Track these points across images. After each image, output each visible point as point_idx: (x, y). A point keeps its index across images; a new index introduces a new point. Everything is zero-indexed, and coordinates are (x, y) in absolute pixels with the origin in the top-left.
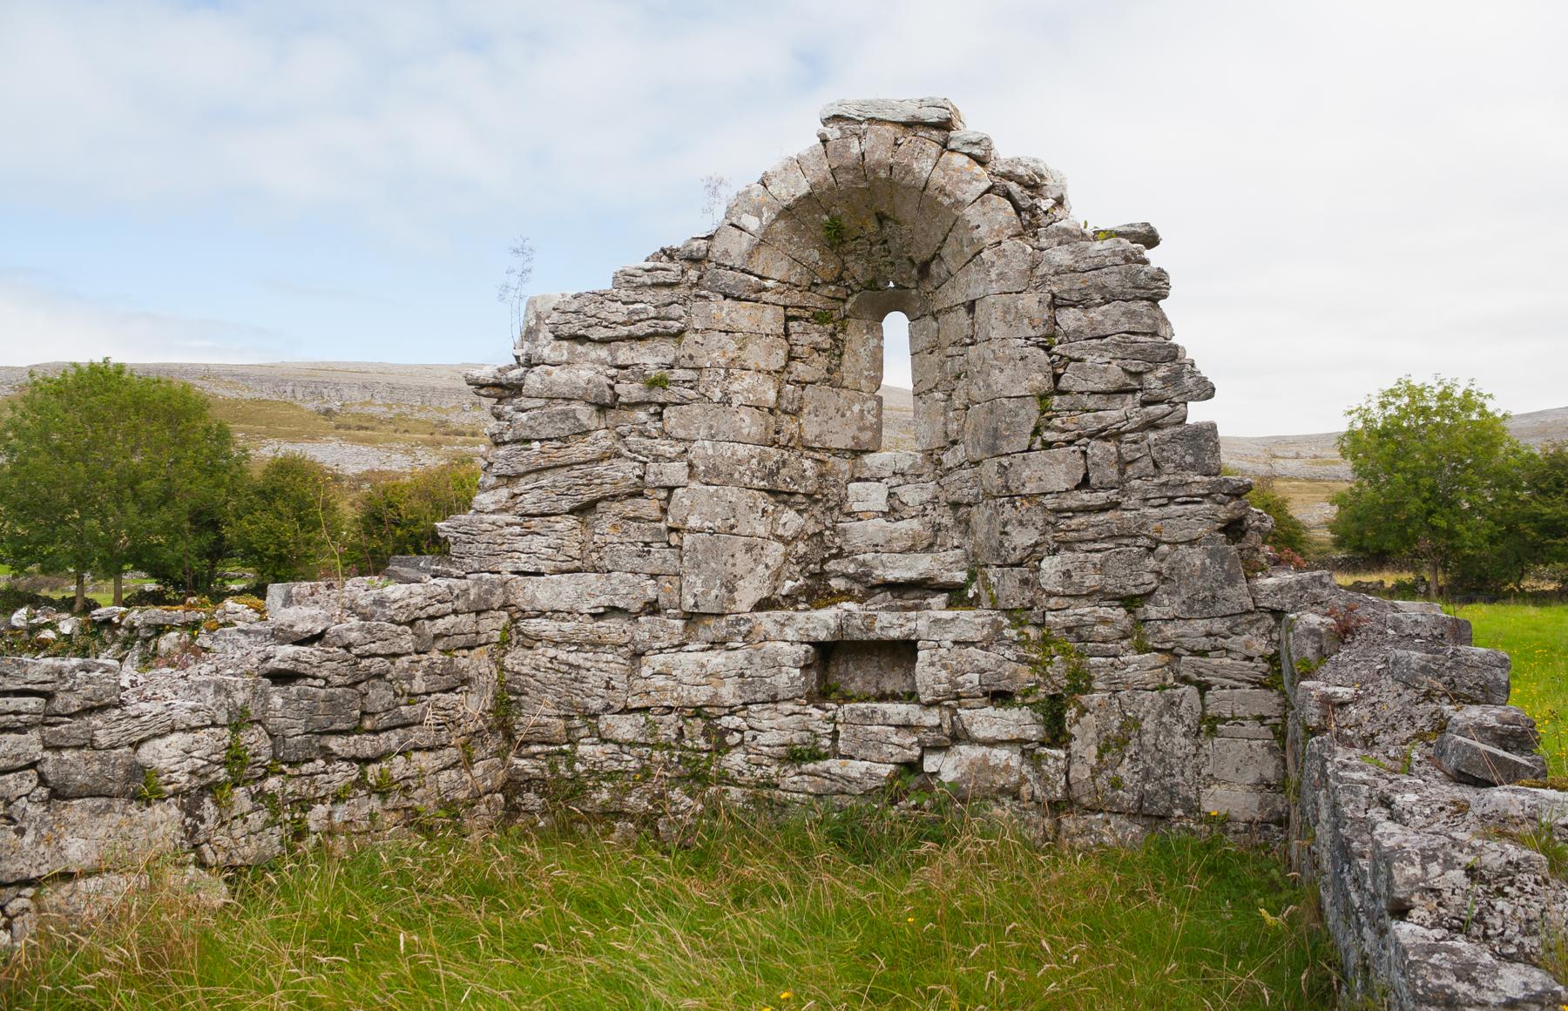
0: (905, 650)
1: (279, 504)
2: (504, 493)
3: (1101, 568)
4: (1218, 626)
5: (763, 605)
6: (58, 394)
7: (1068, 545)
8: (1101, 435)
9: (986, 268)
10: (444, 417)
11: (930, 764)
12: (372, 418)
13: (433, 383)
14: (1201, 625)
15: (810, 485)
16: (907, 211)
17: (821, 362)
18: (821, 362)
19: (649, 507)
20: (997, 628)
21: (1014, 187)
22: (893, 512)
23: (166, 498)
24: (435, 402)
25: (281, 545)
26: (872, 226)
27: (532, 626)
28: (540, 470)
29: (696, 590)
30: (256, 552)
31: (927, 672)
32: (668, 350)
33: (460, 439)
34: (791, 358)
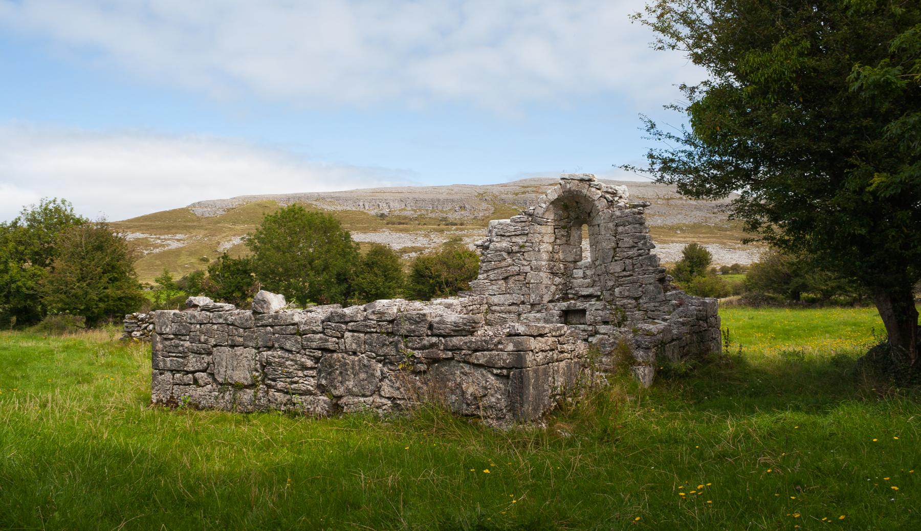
0: (583, 312)
1: (376, 269)
2: (485, 275)
3: (628, 291)
4: (657, 304)
5: (550, 302)
6: (274, 222)
7: (621, 285)
8: (628, 258)
9: (600, 216)
10: (445, 215)
11: (590, 340)
12: (405, 218)
13: (438, 196)
14: (652, 304)
15: (562, 271)
16: (582, 201)
17: (564, 239)
18: (564, 239)
19: (521, 278)
20: (605, 306)
21: (608, 196)
22: (584, 277)
23: (326, 268)
24: (440, 208)
25: (377, 289)
26: (575, 204)
27: (494, 308)
28: (494, 269)
29: (533, 298)
30: (365, 292)
31: (589, 317)
32: (525, 238)
33: (454, 227)
34: (556, 238)
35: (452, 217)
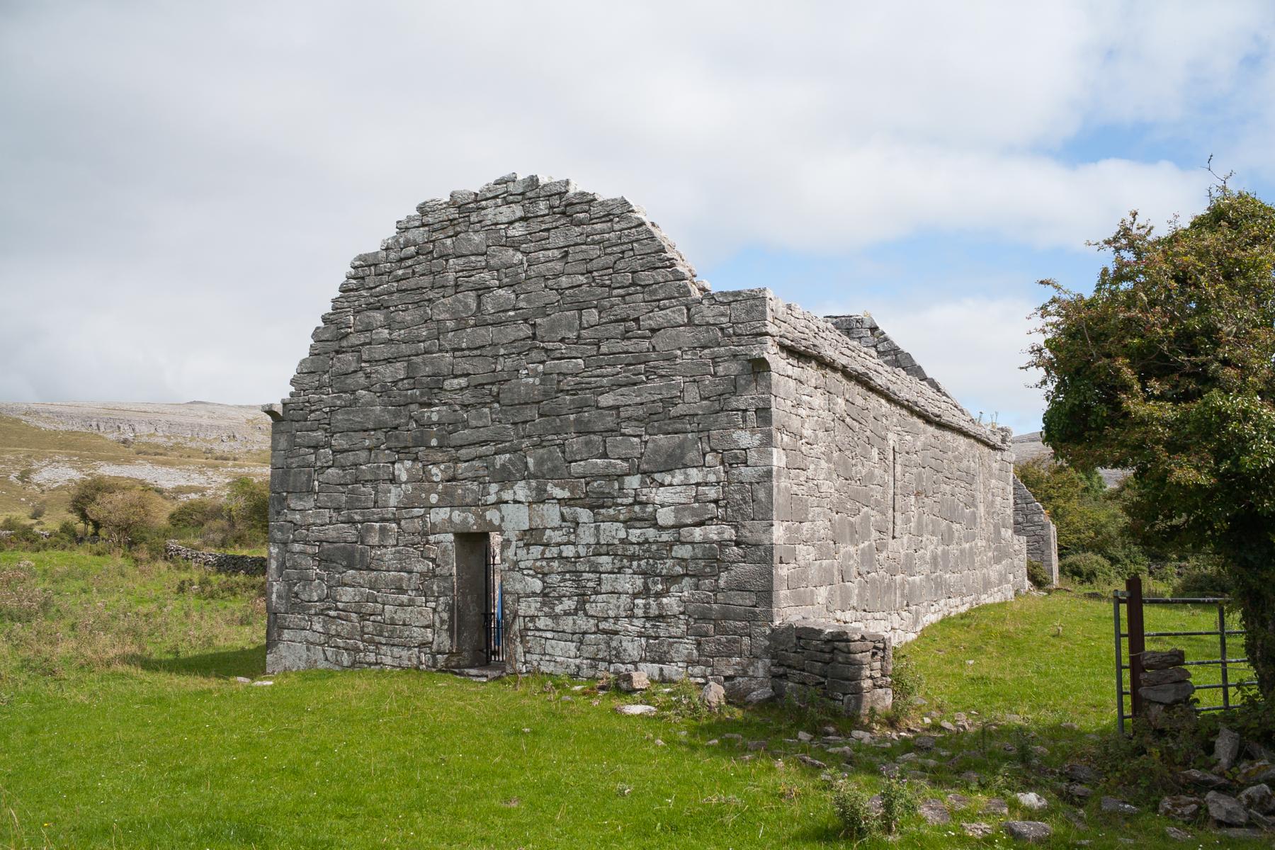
10: (209, 446)
24: (202, 436)
33: (231, 463)
35: (220, 448)
